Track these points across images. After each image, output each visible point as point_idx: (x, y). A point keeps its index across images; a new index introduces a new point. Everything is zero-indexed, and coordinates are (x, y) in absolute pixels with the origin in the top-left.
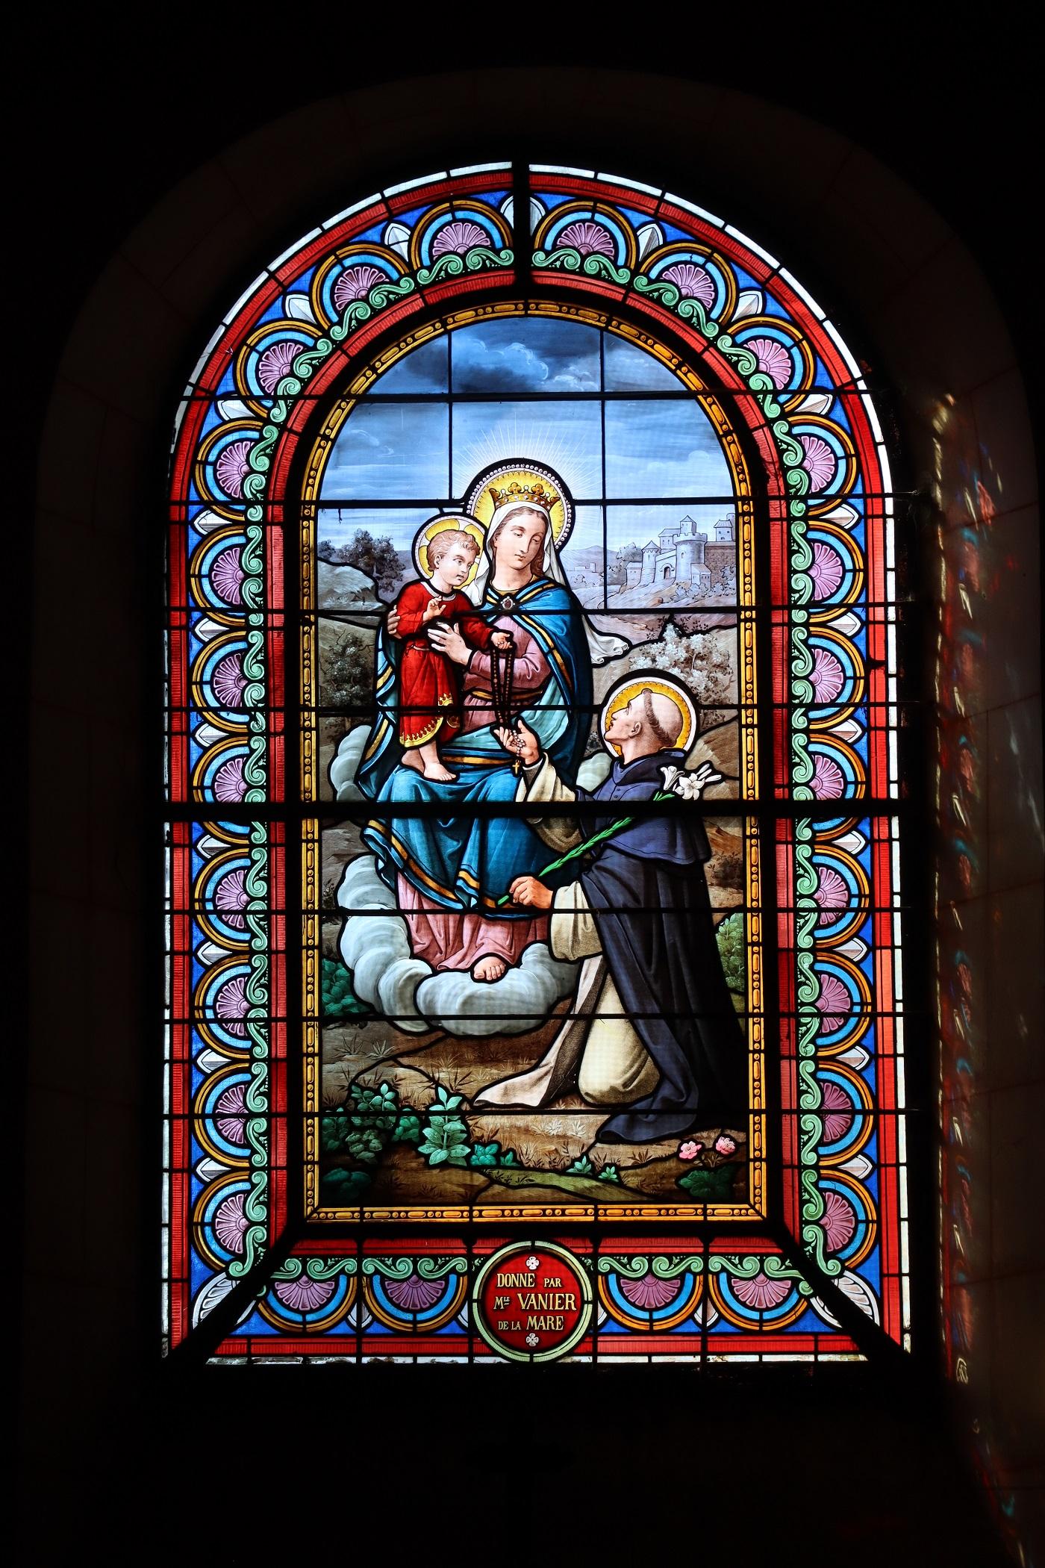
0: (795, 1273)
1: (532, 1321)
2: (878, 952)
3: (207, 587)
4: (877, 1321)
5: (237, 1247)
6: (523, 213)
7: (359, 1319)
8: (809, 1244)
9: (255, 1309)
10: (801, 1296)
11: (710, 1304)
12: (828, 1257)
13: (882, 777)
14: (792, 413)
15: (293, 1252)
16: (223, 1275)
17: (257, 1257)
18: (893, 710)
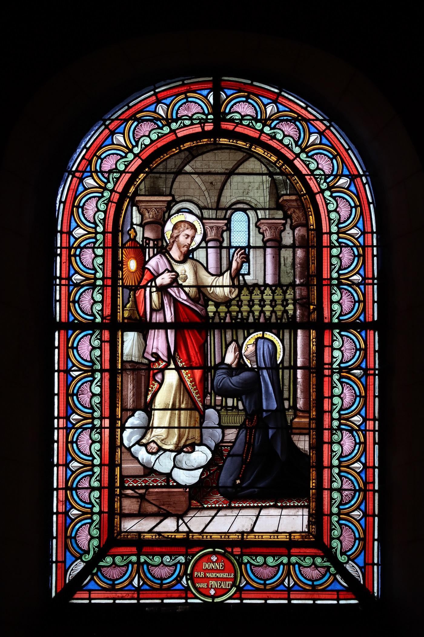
0: (328, 564)
1: (213, 583)
2: (368, 422)
3: (75, 447)
4: (362, 582)
5: (86, 548)
6: (217, 97)
7: (139, 582)
8: (334, 548)
9: (92, 579)
10: (331, 574)
11: (291, 578)
12: (342, 554)
13: (371, 537)
14: (333, 187)
15: (109, 554)
16: (79, 560)
17: (94, 552)
18: (375, 249)
